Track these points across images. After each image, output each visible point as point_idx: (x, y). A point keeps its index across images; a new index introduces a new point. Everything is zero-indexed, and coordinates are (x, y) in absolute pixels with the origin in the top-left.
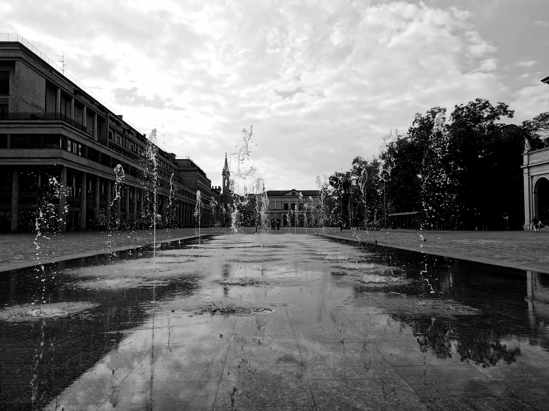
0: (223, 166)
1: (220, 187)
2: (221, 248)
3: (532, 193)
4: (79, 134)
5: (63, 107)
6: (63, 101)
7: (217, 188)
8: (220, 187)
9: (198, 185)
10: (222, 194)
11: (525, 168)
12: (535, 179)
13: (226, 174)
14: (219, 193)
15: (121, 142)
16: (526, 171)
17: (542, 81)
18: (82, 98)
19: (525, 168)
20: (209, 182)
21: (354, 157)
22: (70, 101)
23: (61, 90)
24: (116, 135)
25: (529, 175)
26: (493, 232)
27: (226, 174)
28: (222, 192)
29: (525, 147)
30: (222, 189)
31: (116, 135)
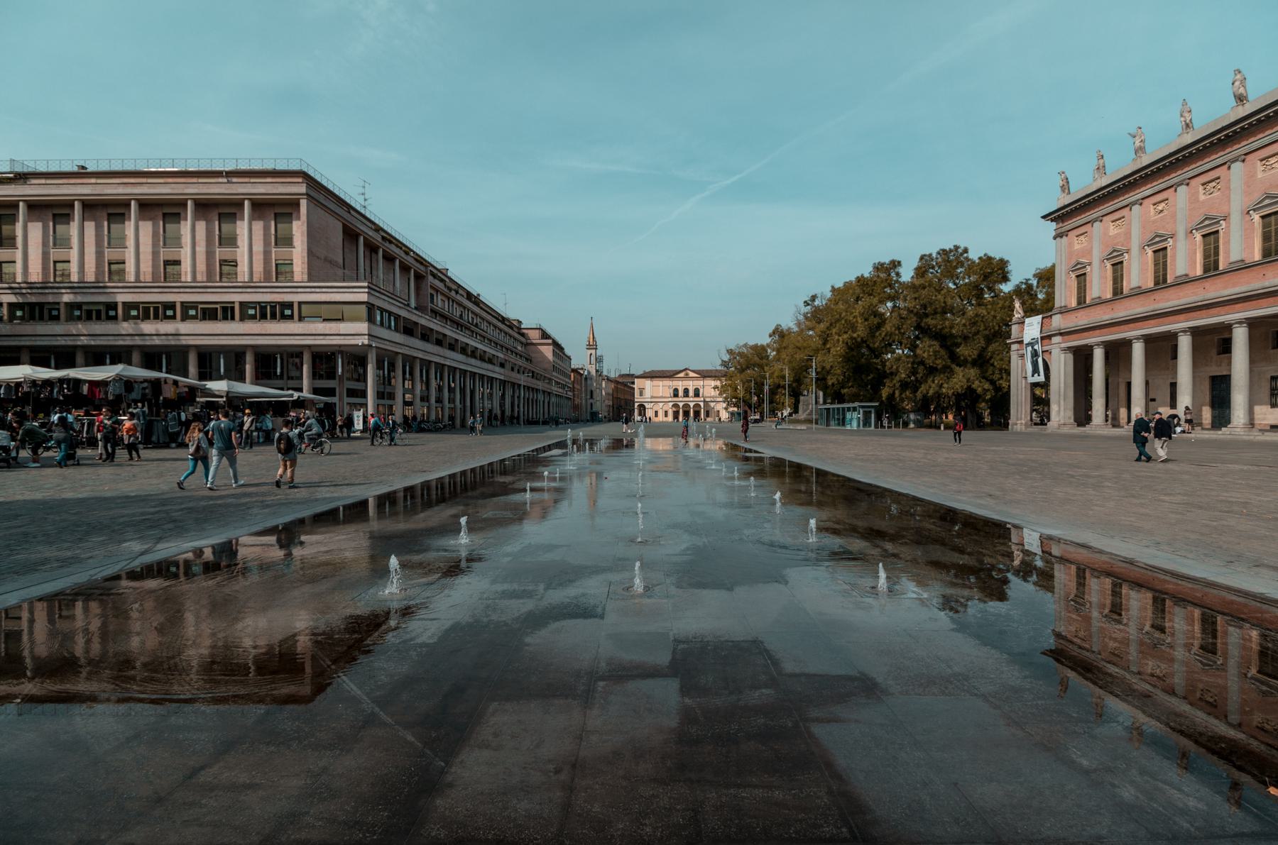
4: (391, 300)
5: (368, 262)
6: (368, 253)
15: (447, 306)
18: (393, 247)
22: (377, 253)
23: (364, 238)
24: (440, 297)
27: (592, 345)
31: (440, 297)
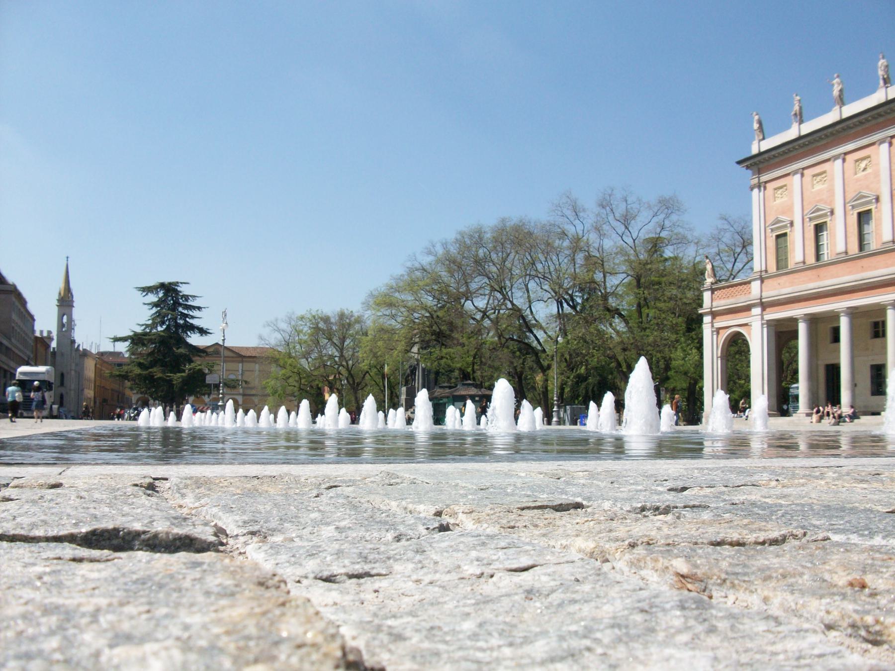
0: (61, 285)
1: (49, 332)
2: (717, 337)
3: (717, 358)
7: (45, 334)
8: (49, 332)
9: (13, 325)
10: (54, 348)
11: (707, 314)
12: (725, 334)
13: (66, 301)
14: (48, 346)
16: (707, 319)
17: (739, 163)
19: (707, 314)
20: (30, 320)
21: (167, 280)
25: (713, 326)
26: (777, 373)
27: (66, 301)
28: (54, 344)
29: (706, 277)
30: (55, 338)
